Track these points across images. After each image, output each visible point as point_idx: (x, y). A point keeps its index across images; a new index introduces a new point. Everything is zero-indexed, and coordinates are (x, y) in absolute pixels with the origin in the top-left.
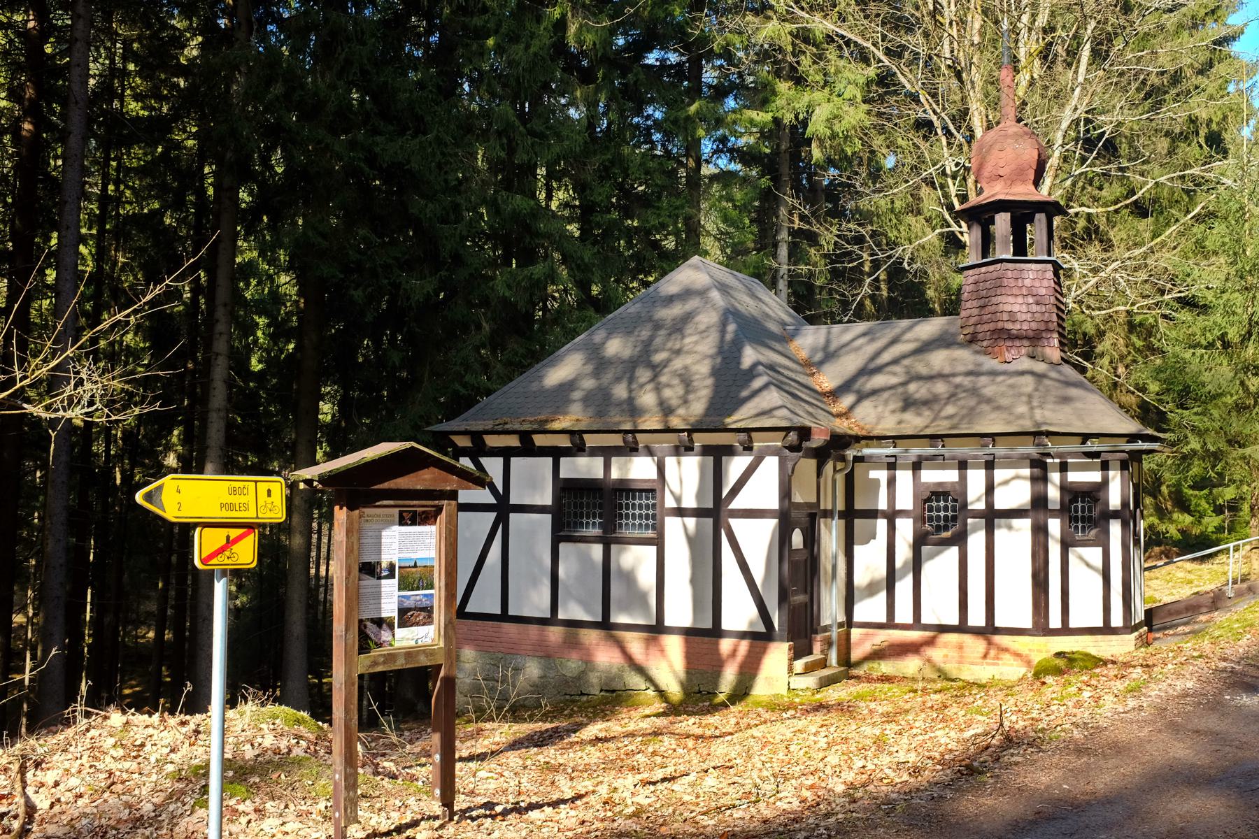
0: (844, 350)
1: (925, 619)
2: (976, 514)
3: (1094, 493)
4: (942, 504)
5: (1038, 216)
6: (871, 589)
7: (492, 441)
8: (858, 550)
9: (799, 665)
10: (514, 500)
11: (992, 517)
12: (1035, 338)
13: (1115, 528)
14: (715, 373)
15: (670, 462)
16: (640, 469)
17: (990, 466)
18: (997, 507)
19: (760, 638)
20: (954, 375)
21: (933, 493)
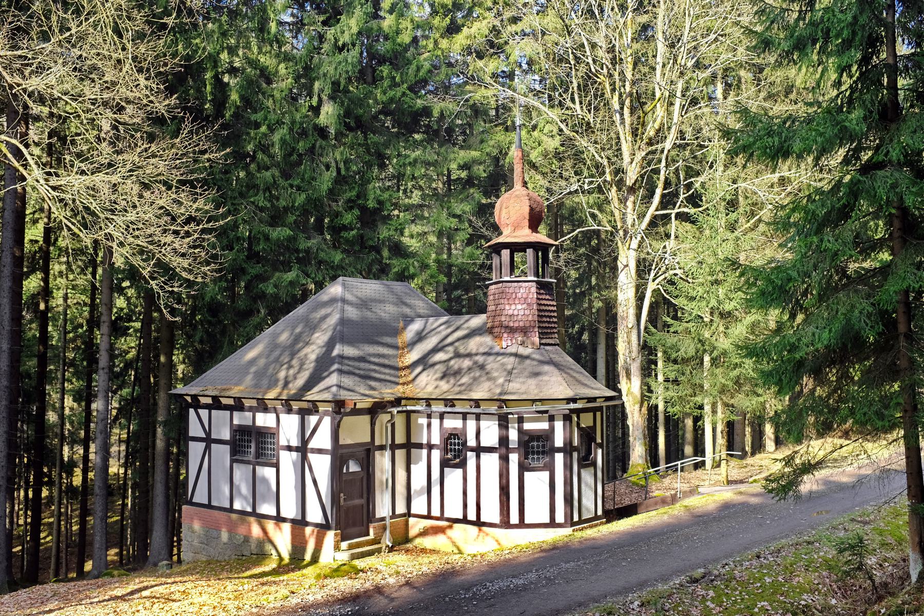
0: (433, 333)
1: (446, 515)
2: (472, 450)
3: (548, 436)
4: (457, 441)
7: (204, 400)
9: (344, 545)
10: (213, 436)
11: (479, 450)
12: (524, 331)
13: (559, 458)
14: (318, 360)
15: (283, 417)
16: (264, 420)
17: (478, 417)
18: (482, 445)
19: (323, 528)
20: (476, 354)
21: (451, 434)
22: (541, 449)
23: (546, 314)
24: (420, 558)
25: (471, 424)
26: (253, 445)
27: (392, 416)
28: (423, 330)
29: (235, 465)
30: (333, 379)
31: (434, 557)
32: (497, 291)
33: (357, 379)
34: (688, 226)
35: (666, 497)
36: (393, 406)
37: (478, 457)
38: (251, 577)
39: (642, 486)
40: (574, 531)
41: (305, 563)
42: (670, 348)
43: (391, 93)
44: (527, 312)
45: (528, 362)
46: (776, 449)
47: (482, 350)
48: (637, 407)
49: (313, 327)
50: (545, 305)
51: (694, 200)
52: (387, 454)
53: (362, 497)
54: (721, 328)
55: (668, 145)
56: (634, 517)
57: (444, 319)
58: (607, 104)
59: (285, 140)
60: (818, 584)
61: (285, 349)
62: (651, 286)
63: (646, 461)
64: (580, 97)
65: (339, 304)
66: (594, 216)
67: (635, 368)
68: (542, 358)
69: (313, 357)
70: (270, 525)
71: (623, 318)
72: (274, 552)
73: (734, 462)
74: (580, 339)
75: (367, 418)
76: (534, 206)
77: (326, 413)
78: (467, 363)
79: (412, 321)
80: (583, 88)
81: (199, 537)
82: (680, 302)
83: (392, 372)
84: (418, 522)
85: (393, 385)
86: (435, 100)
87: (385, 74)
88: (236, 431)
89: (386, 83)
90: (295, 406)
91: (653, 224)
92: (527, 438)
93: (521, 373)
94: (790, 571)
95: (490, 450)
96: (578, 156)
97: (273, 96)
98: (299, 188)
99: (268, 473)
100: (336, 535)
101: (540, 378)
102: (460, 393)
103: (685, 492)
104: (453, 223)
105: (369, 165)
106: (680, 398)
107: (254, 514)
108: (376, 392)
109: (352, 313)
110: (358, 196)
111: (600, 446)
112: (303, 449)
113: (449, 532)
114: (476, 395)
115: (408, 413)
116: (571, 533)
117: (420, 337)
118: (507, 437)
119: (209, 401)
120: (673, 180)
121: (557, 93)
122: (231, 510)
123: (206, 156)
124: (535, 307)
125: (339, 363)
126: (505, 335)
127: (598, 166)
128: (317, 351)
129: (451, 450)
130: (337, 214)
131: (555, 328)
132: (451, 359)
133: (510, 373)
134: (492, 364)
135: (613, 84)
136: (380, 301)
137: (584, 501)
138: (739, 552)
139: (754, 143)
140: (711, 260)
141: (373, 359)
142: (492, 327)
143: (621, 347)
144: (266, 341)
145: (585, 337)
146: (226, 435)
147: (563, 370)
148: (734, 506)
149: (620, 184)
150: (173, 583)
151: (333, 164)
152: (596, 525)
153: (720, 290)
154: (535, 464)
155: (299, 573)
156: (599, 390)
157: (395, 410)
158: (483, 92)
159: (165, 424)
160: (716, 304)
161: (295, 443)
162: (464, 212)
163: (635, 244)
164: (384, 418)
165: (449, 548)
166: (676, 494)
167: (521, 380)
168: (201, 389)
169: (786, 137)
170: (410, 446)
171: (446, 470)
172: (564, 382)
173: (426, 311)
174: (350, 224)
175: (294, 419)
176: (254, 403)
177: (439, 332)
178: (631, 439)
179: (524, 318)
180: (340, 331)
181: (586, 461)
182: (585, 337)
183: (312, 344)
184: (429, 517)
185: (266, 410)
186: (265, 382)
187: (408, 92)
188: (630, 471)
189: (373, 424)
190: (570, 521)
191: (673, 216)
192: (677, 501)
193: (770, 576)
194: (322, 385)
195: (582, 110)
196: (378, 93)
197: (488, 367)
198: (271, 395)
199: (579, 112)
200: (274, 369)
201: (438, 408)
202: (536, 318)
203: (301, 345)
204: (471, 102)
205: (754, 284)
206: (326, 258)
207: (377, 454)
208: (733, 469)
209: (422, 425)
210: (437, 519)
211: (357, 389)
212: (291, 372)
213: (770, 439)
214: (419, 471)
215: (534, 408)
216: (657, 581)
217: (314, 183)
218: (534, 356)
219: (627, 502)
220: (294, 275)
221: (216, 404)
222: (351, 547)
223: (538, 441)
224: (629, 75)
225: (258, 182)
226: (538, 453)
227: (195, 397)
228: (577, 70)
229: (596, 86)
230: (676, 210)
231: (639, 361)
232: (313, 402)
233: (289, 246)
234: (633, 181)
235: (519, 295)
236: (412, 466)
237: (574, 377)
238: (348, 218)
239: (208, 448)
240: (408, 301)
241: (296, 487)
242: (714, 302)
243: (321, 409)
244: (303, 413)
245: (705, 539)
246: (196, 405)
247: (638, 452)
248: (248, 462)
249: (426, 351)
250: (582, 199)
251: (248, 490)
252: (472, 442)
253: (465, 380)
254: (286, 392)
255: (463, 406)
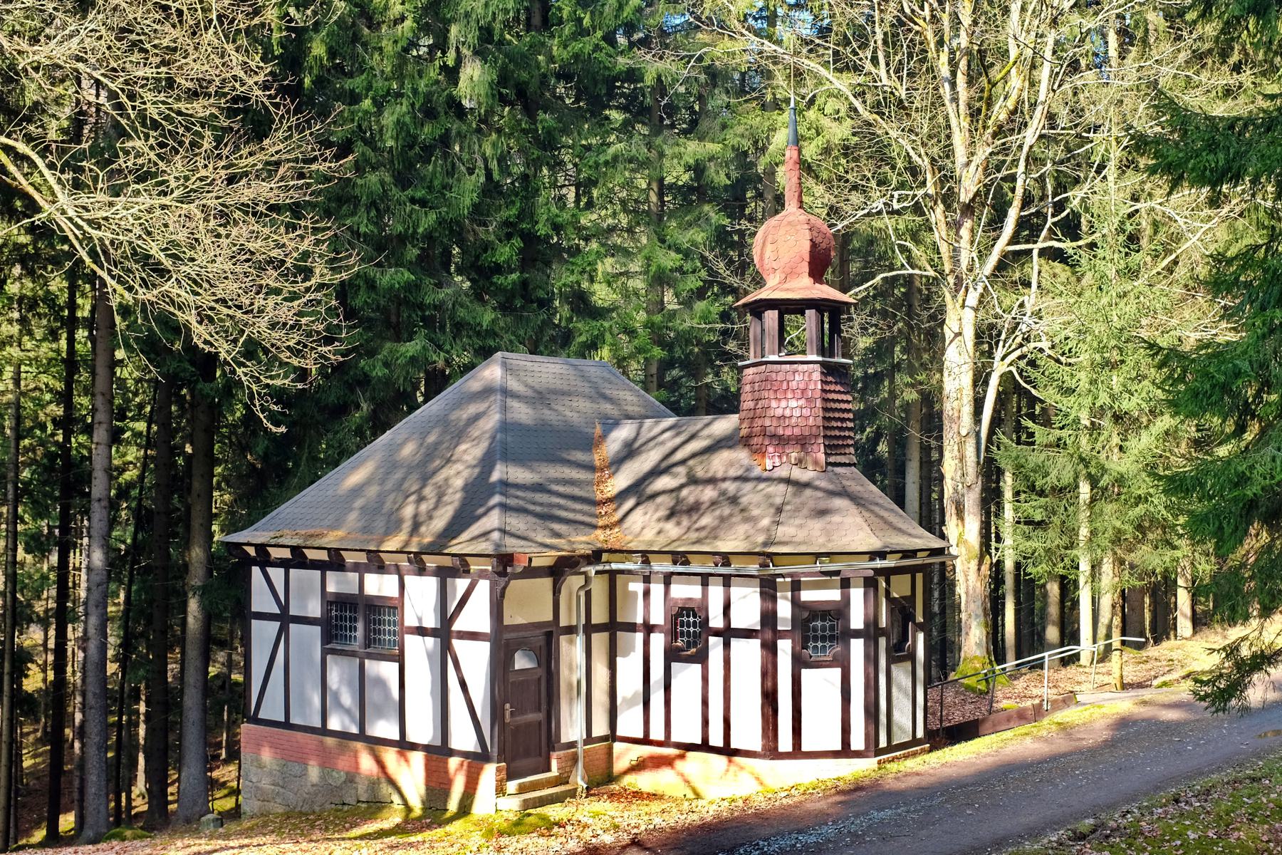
0: (652, 444)
2: (717, 633)
3: (840, 611)
4: (691, 619)
5: (807, 312)
6: (630, 703)
7: (275, 553)
8: (620, 661)
9: (512, 786)
11: (728, 634)
12: (803, 442)
13: (857, 647)
14: (466, 488)
16: (379, 585)
17: (727, 581)
18: (733, 626)
19: (477, 760)
20: (724, 480)
21: (682, 609)
22: (828, 633)
23: (837, 415)
24: (634, 807)
25: (716, 593)
26: (360, 626)
27: (588, 580)
28: (635, 439)
29: (329, 657)
30: (493, 520)
31: (655, 806)
32: (757, 378)
33: (534, 520)
34: (1058, 267)
35: (1025, 709)
36: (590, 564)
37: (727, 646)
38: (362, 837)
39: (981, 692)
40: (879, 762)
41: (448, 815)
42: (1034, 471)
43: (576, 46)
44: (806, 412)
45: (808, 492)
46: (1195, 632)
47: (733, 472)
48: (973, 564)
49: (459, 434)
50: (834, 401)
51: (1071, 228)
52: (580, 640)
53: (540, 710)
54: (1116, 440)
55: (1030, 136)
56: (977, 741)
57: (671, 421)
58: (931, 70)
59: (404, 123)
60: (1268, 842)
61: (410, 469)
62: (999, 368)
63: (988, 652)
64: (887, 56)
65: (499, 397)
66: (904, 249)
67: (972, 500)
68: (831, 487)
69: (458, 483)
70: (390, 756)
71: (952, 420)
72: (396, 799)
73: (1130, 654)
74: (874, 450)
75: (547, 582)
76: (818, 240)
77: (482, 574)
78: (708, 493)
79: (616, 424)
80: (891, 41)
81: (271, 773)
82: (1048, 395)
83: (586, 508)
84: (628, 750)
85: (587, 530)
86: (648, 57)
87: (565, 14)
88: (331, 603)
89: (568, 29)
90: (431, 562)
91: (1001, 266)
92: (806, 615)
93: (797, 510)
94: (1226, 824)
95: (747, 634)
96: (881, 154)
97: (381, 49)
98: (423, 203)
99: (388, 670)
100: (498, 770)
101: (828, 518)
102: (698, 541)
103: (1055, 702)
104: (669, 260)
105: (536, 164)
106: (1048, 551)
107: (362, 736)
108: (563, 541)
109: (522, 413)
110: (521, 216)
111: (920, 627)
112: (444, 633)
113: (679, 764)
114: (725, 546)
115: (613, 575)
116: (876, 766)
117: (630, 451)
118: (775, 613)
119: (286, 554)
120: (1036, 193)
121: (849, 50)
122: (324, 731)
123: (314, 167)
124: (819, 404)
125: (501, 494)
126: (771, 449)
127: (914, 170)
128: (466, 473)
129: (682, 634)
130: (486, 246)
131: (849, 437)
132: (682, 486)
133: (779, 510)
134: (750, 495)
135: (939, 33)
136: (564, 393)
137: (897, 715)
138: (1146, 794)
139: (1188, 161)
140: (1099, 328)
141: (555, 487)
142: (749, 436)
143: (949, 467)
144: (379, 456)
145: (883, 448)
146: (314, 609)
147: (863, 506)
148: (1135, 722)
149: (948, 199)
150: (241, 847)
151: (480, 163)
152: (914, 754)
153: (1115, 378)
154: (819, 656)
155: (439, 832)
156: (924, 540)
157: (591, 570)
158: (726, 45)
159: (204, 591)
160: (1108, 401)
161: (431, 622)
162: (694, 244)
163: (973, 299)
164: (573, 582)
165: (678, 790)
166: (1041, 705)
167: (798, 522)
168: (272, 534)
169: (1237, 153)
170: (614, 627)
171: (675, 666)
172: (865, 525)
173: (637, 409)
174: (508, 262)
175: (429, 585)
176: (362, 558)
177: (662, 443)
178: (963, 616)
179: (802, 422)
180: (501, 442)
181: (899, 652)
182: (883, 448)
183: (457, 461)
184: (646, 741)
185: (381, 568)
186: (380, 524)
187: (603, 44)
188: (961, 667)
189: (556, 592)
190: (873, 748)
191: (1035, 253)
192: (1043, 716)
193: (1196, 830)
194: (475, 529)
195: (889, 77)
196: (555, 46)
197: (744, 500)
198: (392, 544)
199: (885, 81)
200: (394, 502)
201: (662, 566)
202: (820, 422)
203: (437, 462)
204: (707, 62)
205: (1182, 379)
206: (469, 318)
207: (563, 640)
208: (1122, 664)
209: (635, 593)
210: (659, 744)
211: (532, 535)
212: (424, 507)
213: (1185, 616)
214: (629, 668)
215: (819, 567)
216: (1022, 837)
217: (448, 195)
218: (817, 483)
219: (957, 717)
220: (419, 347)
221: (298, 559)
222: (522, 789)
223: (823, 620)
224: (966, 20)
225: (357, 191)
226: (823, 639)
227: (261, 548)
228: (881, 11)
229: (911, 36)
230: (1040, 245)
231: (978, 489)
232: (462, 556)
233: (406, 298)
234: (971, 195)
235: (793, 385)
236: (619, 660)
237: (882, 518)
238: (506, 253)
239: (283, 630)
240: (608, 392)
241: (432, 693)
242: (1104, 398)
243: (473, 568)
244: (444, 574)
245: (1093, 774)
246: (264, 561)
247: (973, 639)
248: (353, 654)
249: (641, 475)
250: (887, 222)
251: (353, 697)
252: (716, 621)
253: (706, 520)
254: (415, 540)
255: (703, 565)
